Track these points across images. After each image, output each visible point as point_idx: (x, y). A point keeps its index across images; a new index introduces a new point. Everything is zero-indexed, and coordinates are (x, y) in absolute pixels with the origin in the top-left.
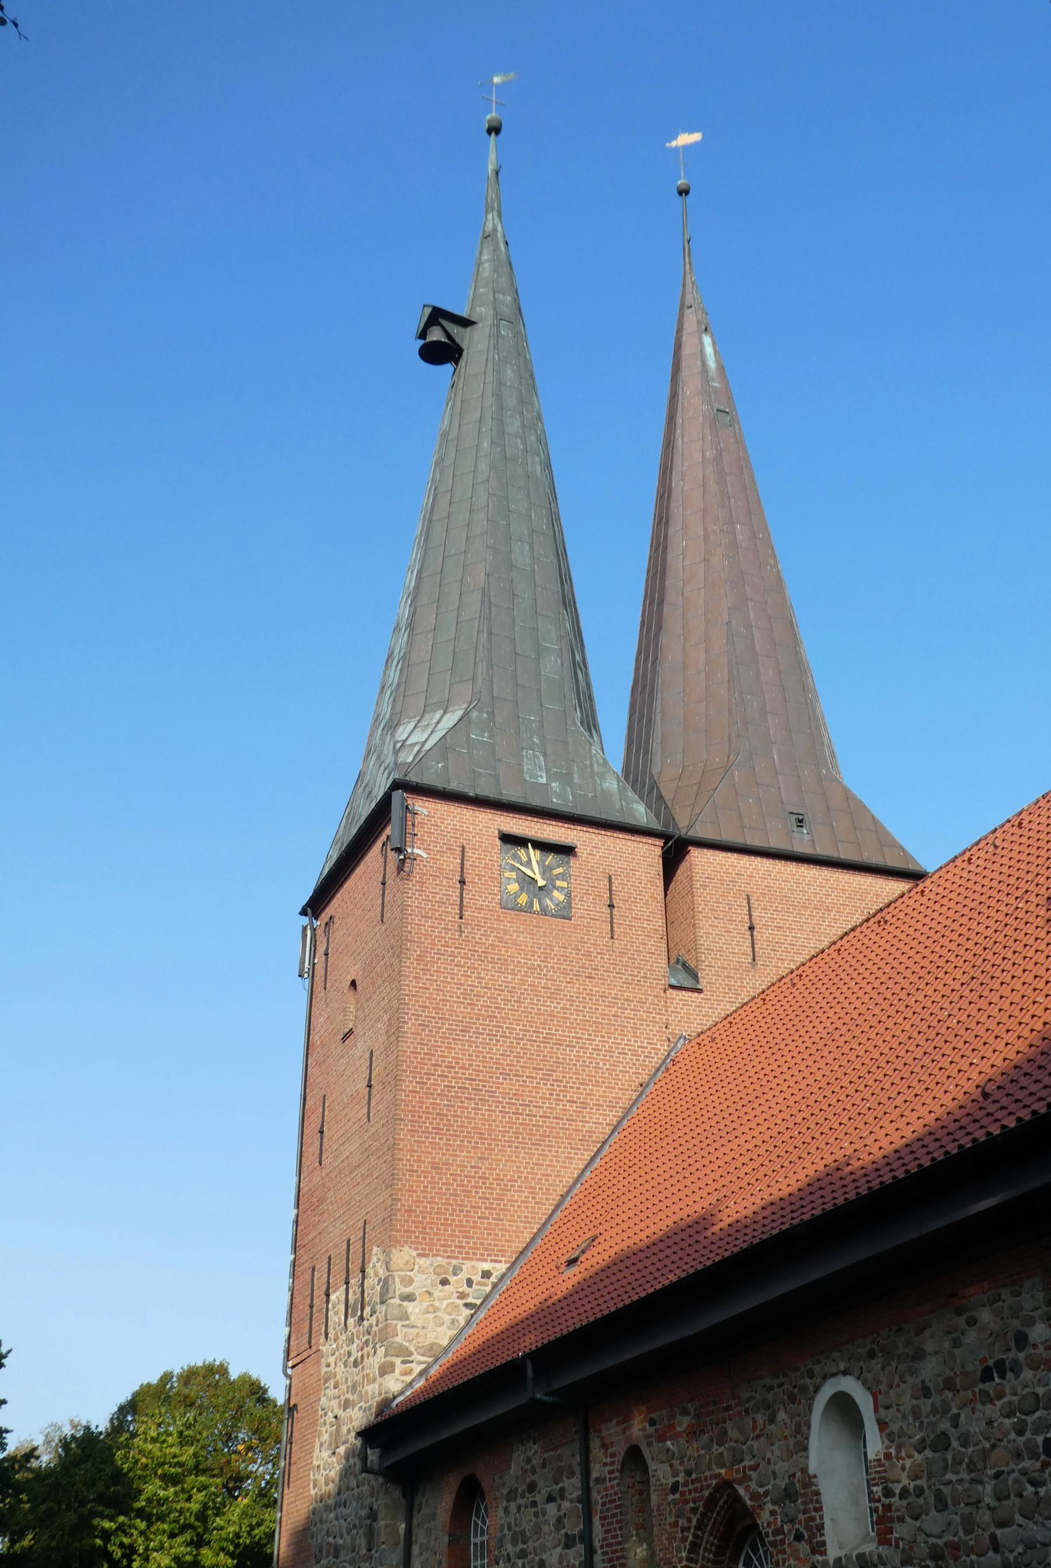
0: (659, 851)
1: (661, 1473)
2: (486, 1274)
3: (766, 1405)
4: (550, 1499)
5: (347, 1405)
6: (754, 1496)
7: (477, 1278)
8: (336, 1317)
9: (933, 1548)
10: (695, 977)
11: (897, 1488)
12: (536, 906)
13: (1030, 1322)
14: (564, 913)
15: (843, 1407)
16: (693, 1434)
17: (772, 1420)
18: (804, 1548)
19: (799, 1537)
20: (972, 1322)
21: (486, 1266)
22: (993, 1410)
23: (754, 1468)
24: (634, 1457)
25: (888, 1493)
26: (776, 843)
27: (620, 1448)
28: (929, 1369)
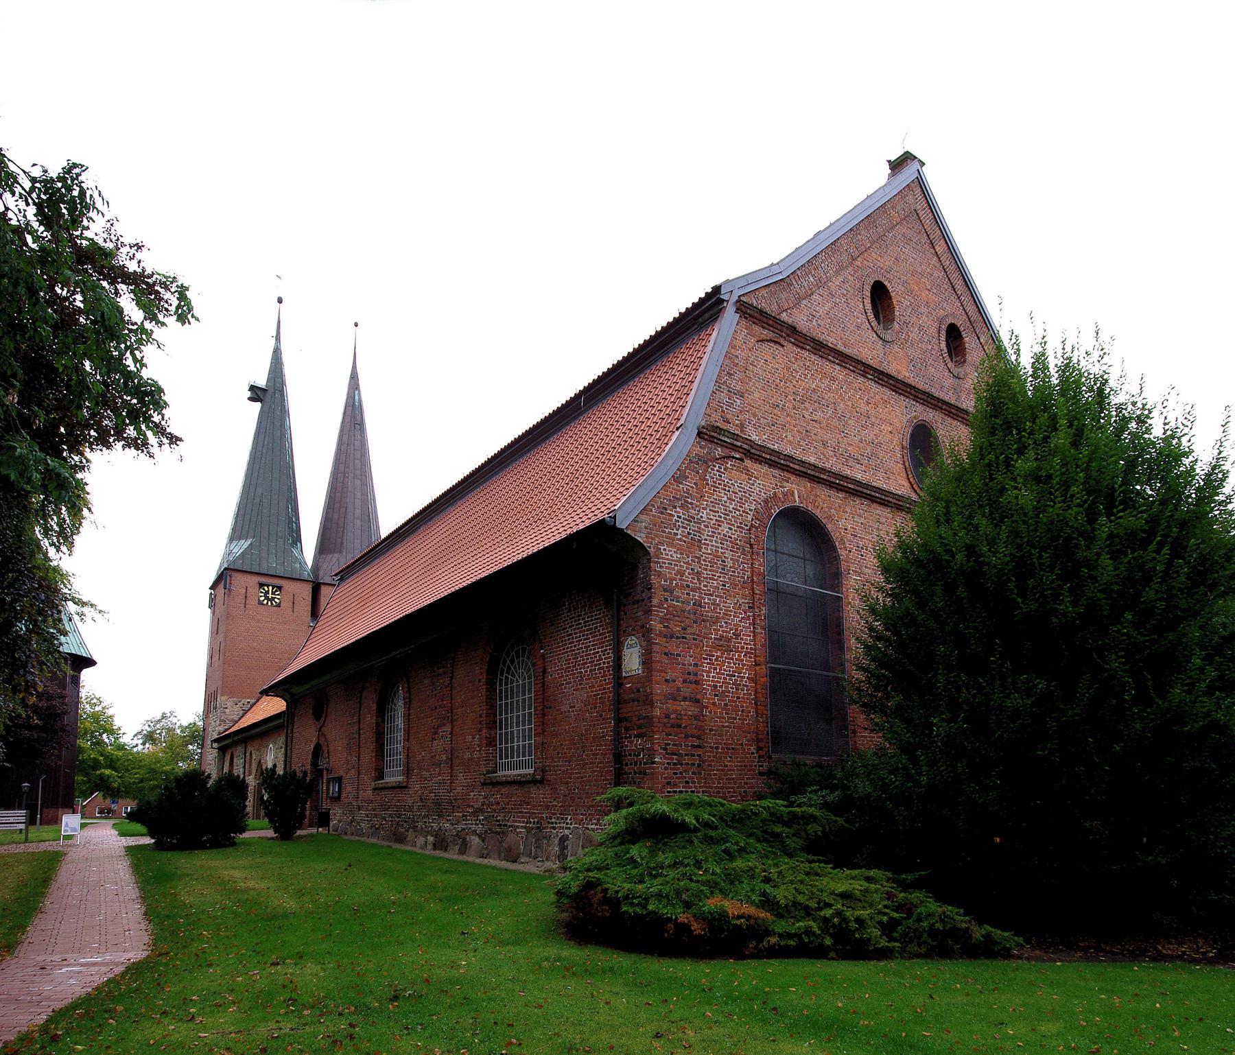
14: (279, 605)
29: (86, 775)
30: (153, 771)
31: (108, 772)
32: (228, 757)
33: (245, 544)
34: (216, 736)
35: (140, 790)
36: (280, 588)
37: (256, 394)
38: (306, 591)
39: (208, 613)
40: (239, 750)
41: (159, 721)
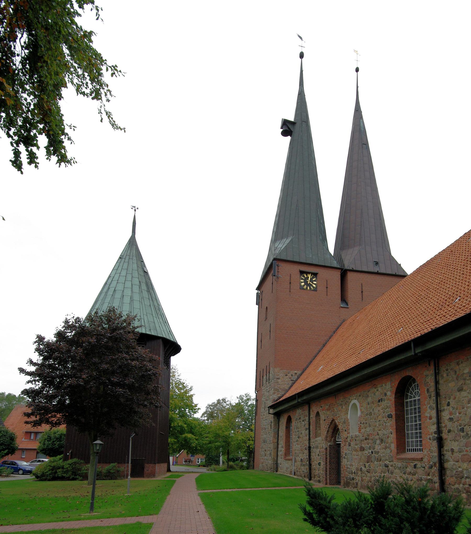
0: (340, 273)
1: (322, 417)
2: (296, 374)
3: (341, 405)
4: (303, 421)
5: (267, 400)
6: (338, 422)
7: (294, 374)
8: (264, 382)
9: (368, 434)
10: (347, 304)
11: (362, 422)
12: (308, 288)
13: (388, 391)
14: (315, 290)
15: (354, 405)
16: (328, 410)
17: (342, 408)
18: (346, 433)
19: (345, 431)
20: (377, 390)
21: (296, 372)
22: (379, 408)
23: (339, 417)
24: (318, 414)
25: (361, 423)
26: (370, 270)
27: (316, 412)
28: (370, 399)
29: (177, 438)
30: (217, 436)
31: (189, 436)
32: (283, 420)
33: (287, 241)
34: (271, 404)
35: (209, 449)
36: (315, 275)
37: (287, 128)
38: (337, 275)
39: (256, 308)
40: (425, 376)
41: (216, 405)
